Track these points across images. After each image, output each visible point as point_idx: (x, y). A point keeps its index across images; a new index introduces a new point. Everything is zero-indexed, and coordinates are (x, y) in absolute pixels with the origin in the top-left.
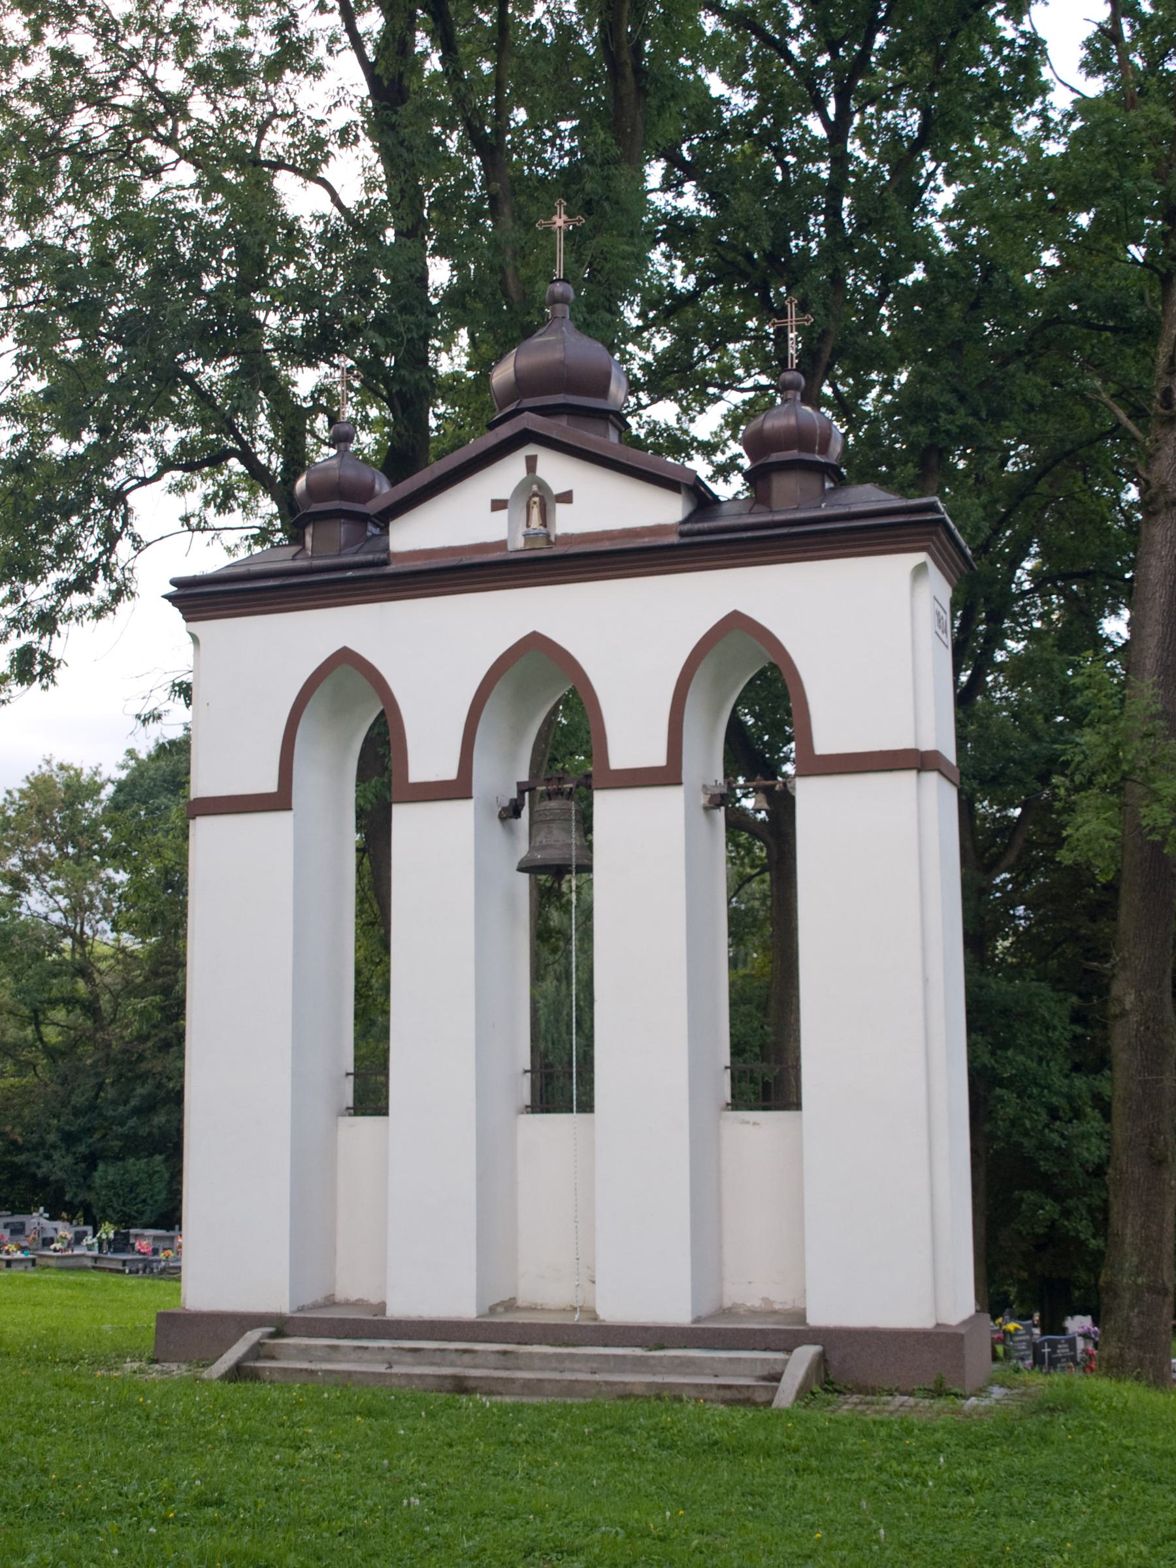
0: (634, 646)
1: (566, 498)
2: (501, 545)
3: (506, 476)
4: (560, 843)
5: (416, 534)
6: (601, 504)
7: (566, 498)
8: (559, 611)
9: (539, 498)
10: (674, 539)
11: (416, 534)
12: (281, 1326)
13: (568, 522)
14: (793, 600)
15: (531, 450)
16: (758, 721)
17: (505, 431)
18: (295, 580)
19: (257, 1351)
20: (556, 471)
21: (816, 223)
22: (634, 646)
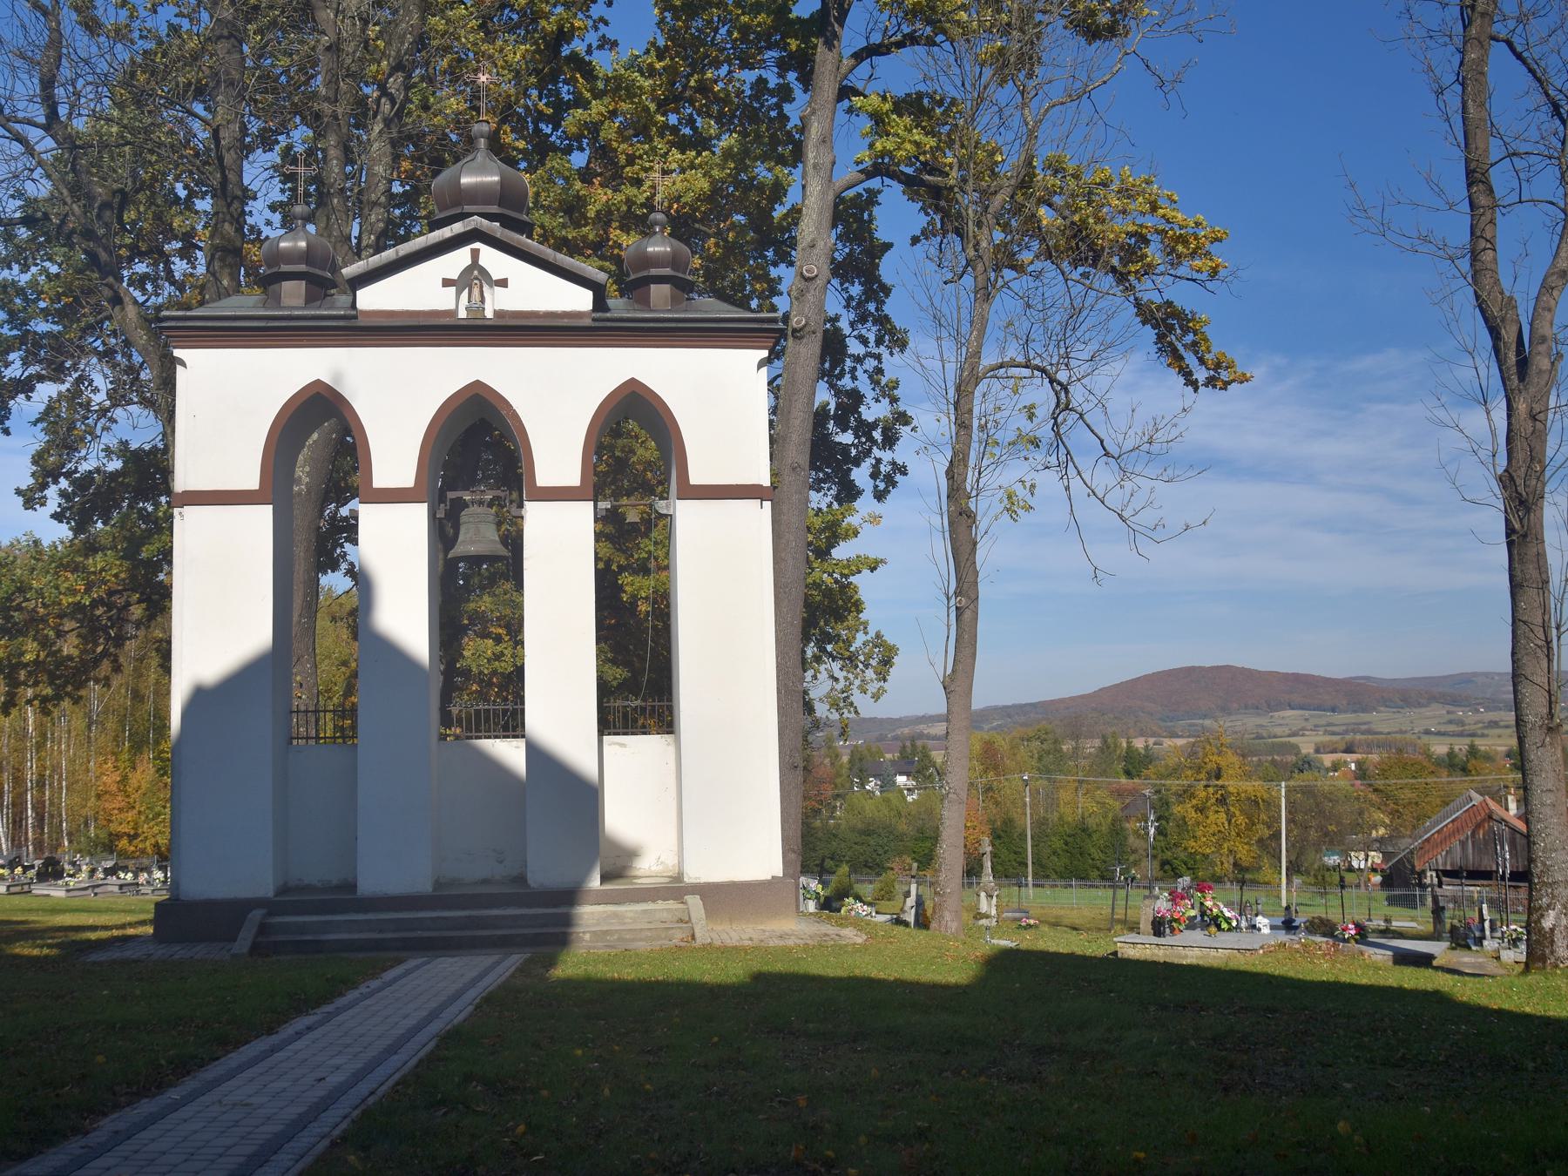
0: (556, 401)
1: (503, 283)
2: (452, 313)
3: (458, 260)
4: (477, 537)
5: (371, 299)
6: (531, 289)
7: (503, 283)
8: (508, 371)
9: (474, 277)
10: (587, 322)
11: (371, 299)
12: (271, 906)
13: (496, 302)
14: (668, 371)
15: (477, 245)
16: (634, 456)
17: (458, 228)
18: (609, 324)
19: (263, 929)
20: (494, 261)
21: (196, 126)
22: (556, 401)
